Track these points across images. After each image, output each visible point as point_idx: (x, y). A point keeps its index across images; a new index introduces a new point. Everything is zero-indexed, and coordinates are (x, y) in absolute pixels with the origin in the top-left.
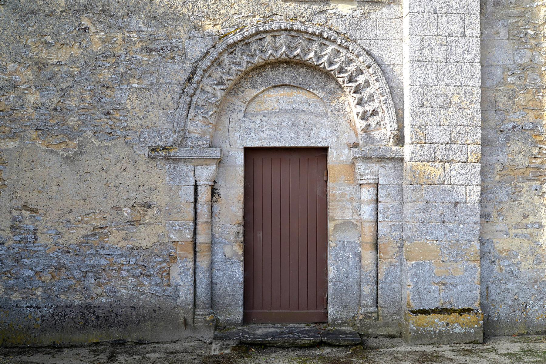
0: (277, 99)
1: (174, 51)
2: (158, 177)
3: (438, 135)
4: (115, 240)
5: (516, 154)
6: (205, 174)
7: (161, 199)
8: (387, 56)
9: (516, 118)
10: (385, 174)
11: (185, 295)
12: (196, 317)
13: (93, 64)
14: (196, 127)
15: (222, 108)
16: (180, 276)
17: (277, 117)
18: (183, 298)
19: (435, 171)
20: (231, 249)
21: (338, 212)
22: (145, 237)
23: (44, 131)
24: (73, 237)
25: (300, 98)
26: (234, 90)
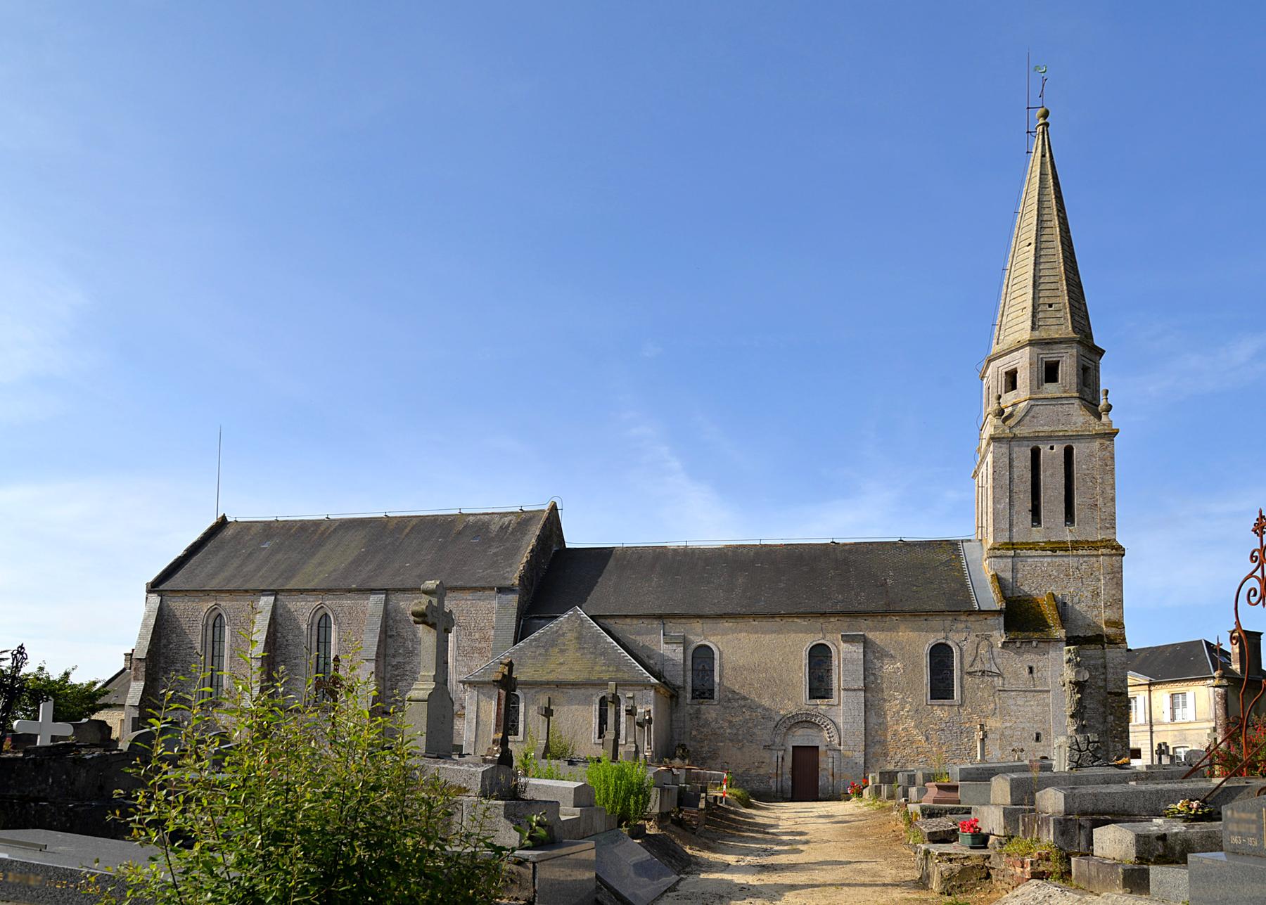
0: (800, 732)
1: (771, 719)
2: (766, 754)
3: (851, 744)
4: (753, 772)
5: (878, 749)
6: (780, 753)
7: (767, 760)
8: (836, 720)
9: (877, 738)
10: (836, 754)
11: (774, 788)
12: (1254, 817)
13: (746, 721)
14: (778, 740)
15: (785, 735)
16: (772, 783)
17: (801, 738)
18: (533, 711)
19: (850, 754)
20: (788, 776)
21: (821, 766)
22: (762, 771)
23: (731, 741)
24: (740, 771)
25: (810, 731)
26: (789, 729)
